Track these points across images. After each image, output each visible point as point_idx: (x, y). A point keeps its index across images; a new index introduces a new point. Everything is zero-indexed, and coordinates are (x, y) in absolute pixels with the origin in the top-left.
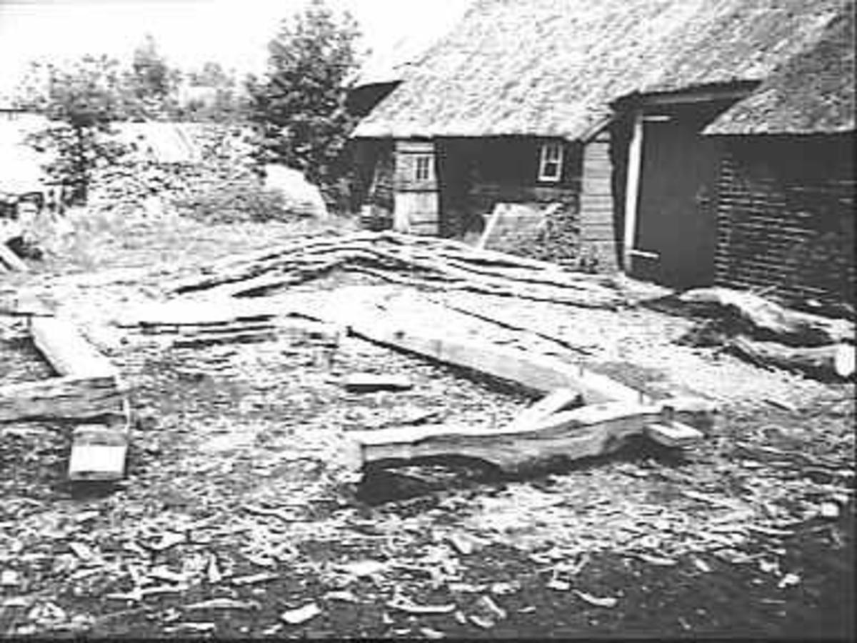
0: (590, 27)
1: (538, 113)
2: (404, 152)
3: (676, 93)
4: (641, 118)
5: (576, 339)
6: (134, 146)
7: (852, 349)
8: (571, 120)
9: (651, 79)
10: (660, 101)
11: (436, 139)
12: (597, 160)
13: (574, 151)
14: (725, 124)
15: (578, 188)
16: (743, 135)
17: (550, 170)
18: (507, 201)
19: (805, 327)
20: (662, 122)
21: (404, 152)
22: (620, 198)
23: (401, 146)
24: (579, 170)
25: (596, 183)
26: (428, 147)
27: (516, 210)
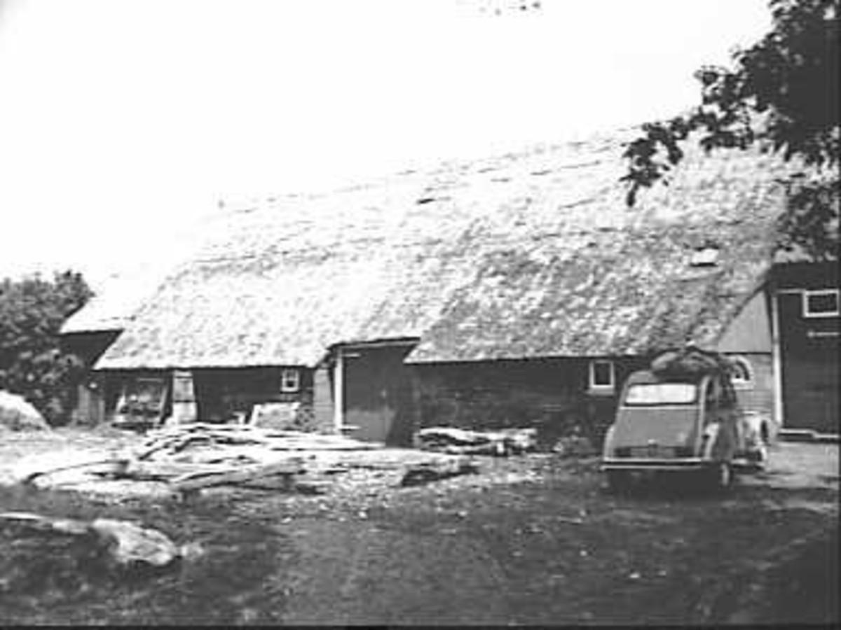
0: (286, 304)
1: (279, 352)
2: (180, 377)
3: (370, 342)
4: (340, 355)
5: (339, 457)
6: (410, 267)
7: (836, 448)
8: (310, 356)
9: (349, 334)
10: (352, 347)
11: (193, 369)
12: (321, 377)
13: (306, 373)
14: (414, 357)
15: (311, 393)
16: (526, 360)
17: (290, 384)
18: (262, 403)
19: (479, 438)
20: (831, 318)
21: (180, 377)
22: (111, 405)
23: (177, 373)
24: (312, 384)
25: (321, 390)
26: (187, 374)
27: (269, 408)
